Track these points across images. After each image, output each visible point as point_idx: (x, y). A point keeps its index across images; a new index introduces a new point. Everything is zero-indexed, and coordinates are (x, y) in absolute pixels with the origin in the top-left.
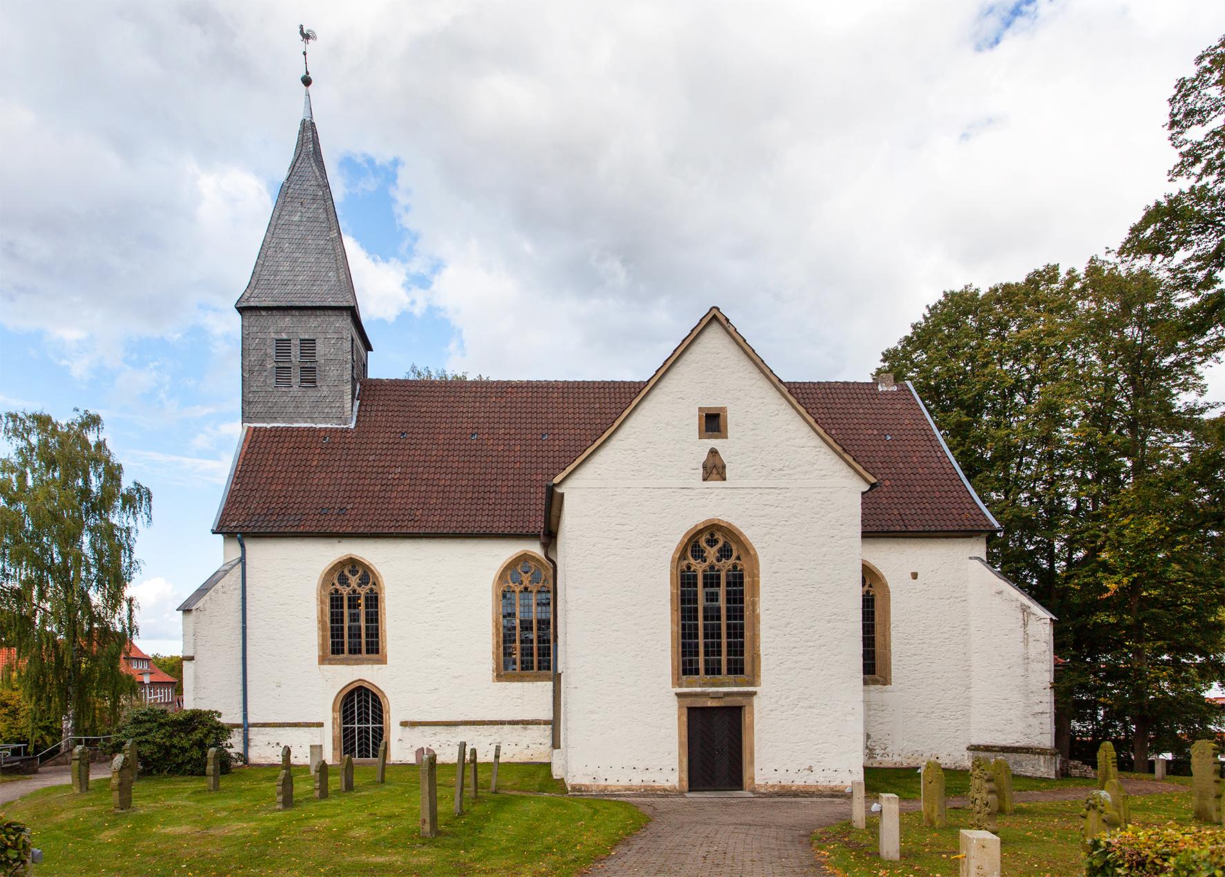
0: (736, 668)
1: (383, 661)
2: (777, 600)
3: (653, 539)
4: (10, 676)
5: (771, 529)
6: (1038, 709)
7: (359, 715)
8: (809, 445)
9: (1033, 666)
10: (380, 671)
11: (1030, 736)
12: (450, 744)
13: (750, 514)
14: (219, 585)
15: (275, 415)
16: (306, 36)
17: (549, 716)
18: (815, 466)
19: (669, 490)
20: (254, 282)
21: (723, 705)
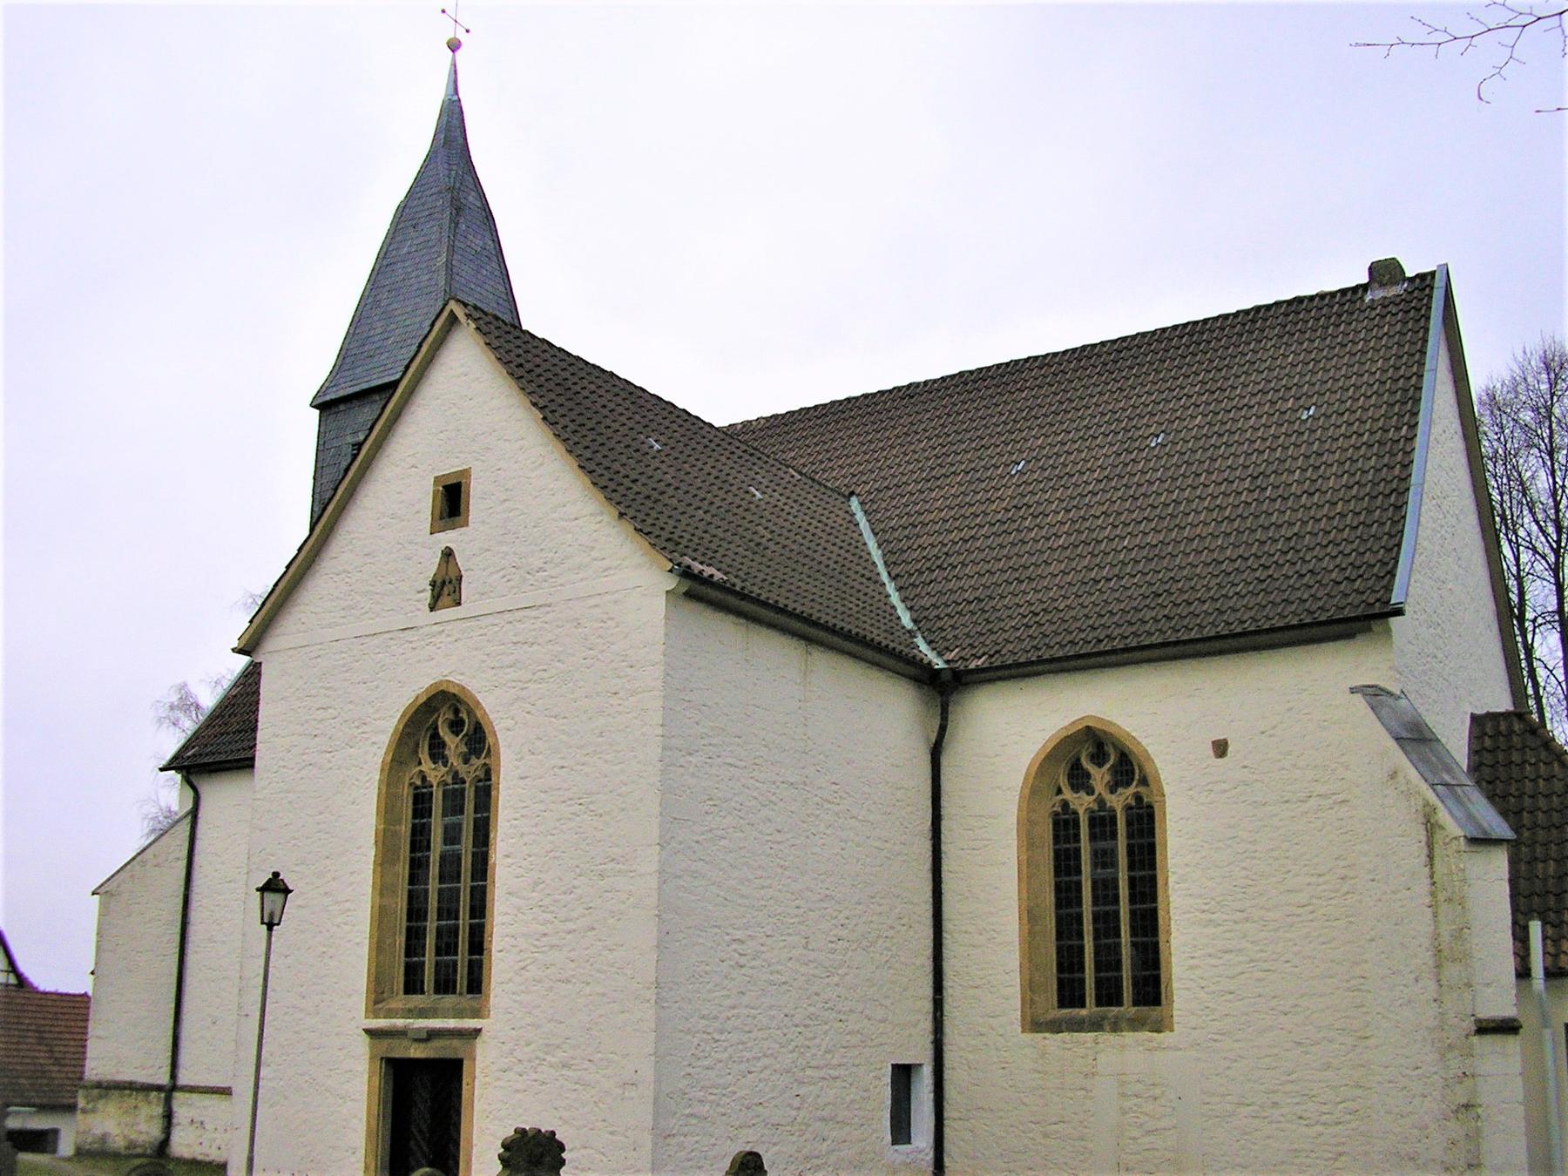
2: (522, 835)
8: (584, 512)
18: (594, 554)
19: (387, 636)
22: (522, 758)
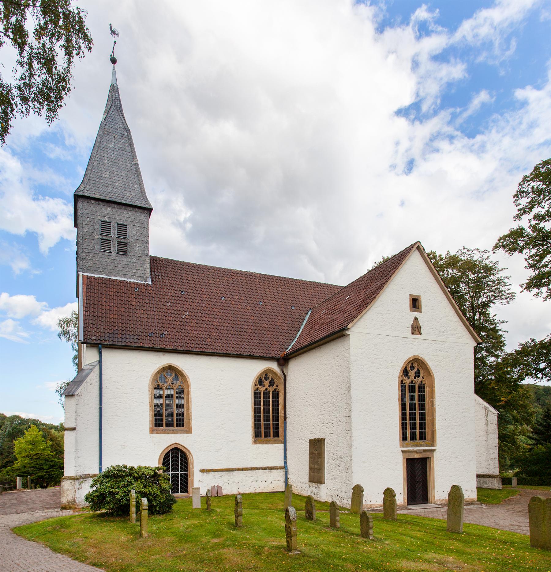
0: (423, 437)
1: (189, 431)
2: (442, 400)
3: (391, 364)
4: (534, 455)
5: (440, 362)
6: (493, 456)
7: (172, 466)
9: (490, 436)
10: (188, 438)
11: (489, 469)
12: (230, 482)
13: (431, 354)
14: (88, 379)
15: (100, 270)
16: (114, 33)
17: (282, 464)
18: (456, 332)
19: (397, 338)
20: (86, 180)
21: (422, 457)
22: (441, 381)
